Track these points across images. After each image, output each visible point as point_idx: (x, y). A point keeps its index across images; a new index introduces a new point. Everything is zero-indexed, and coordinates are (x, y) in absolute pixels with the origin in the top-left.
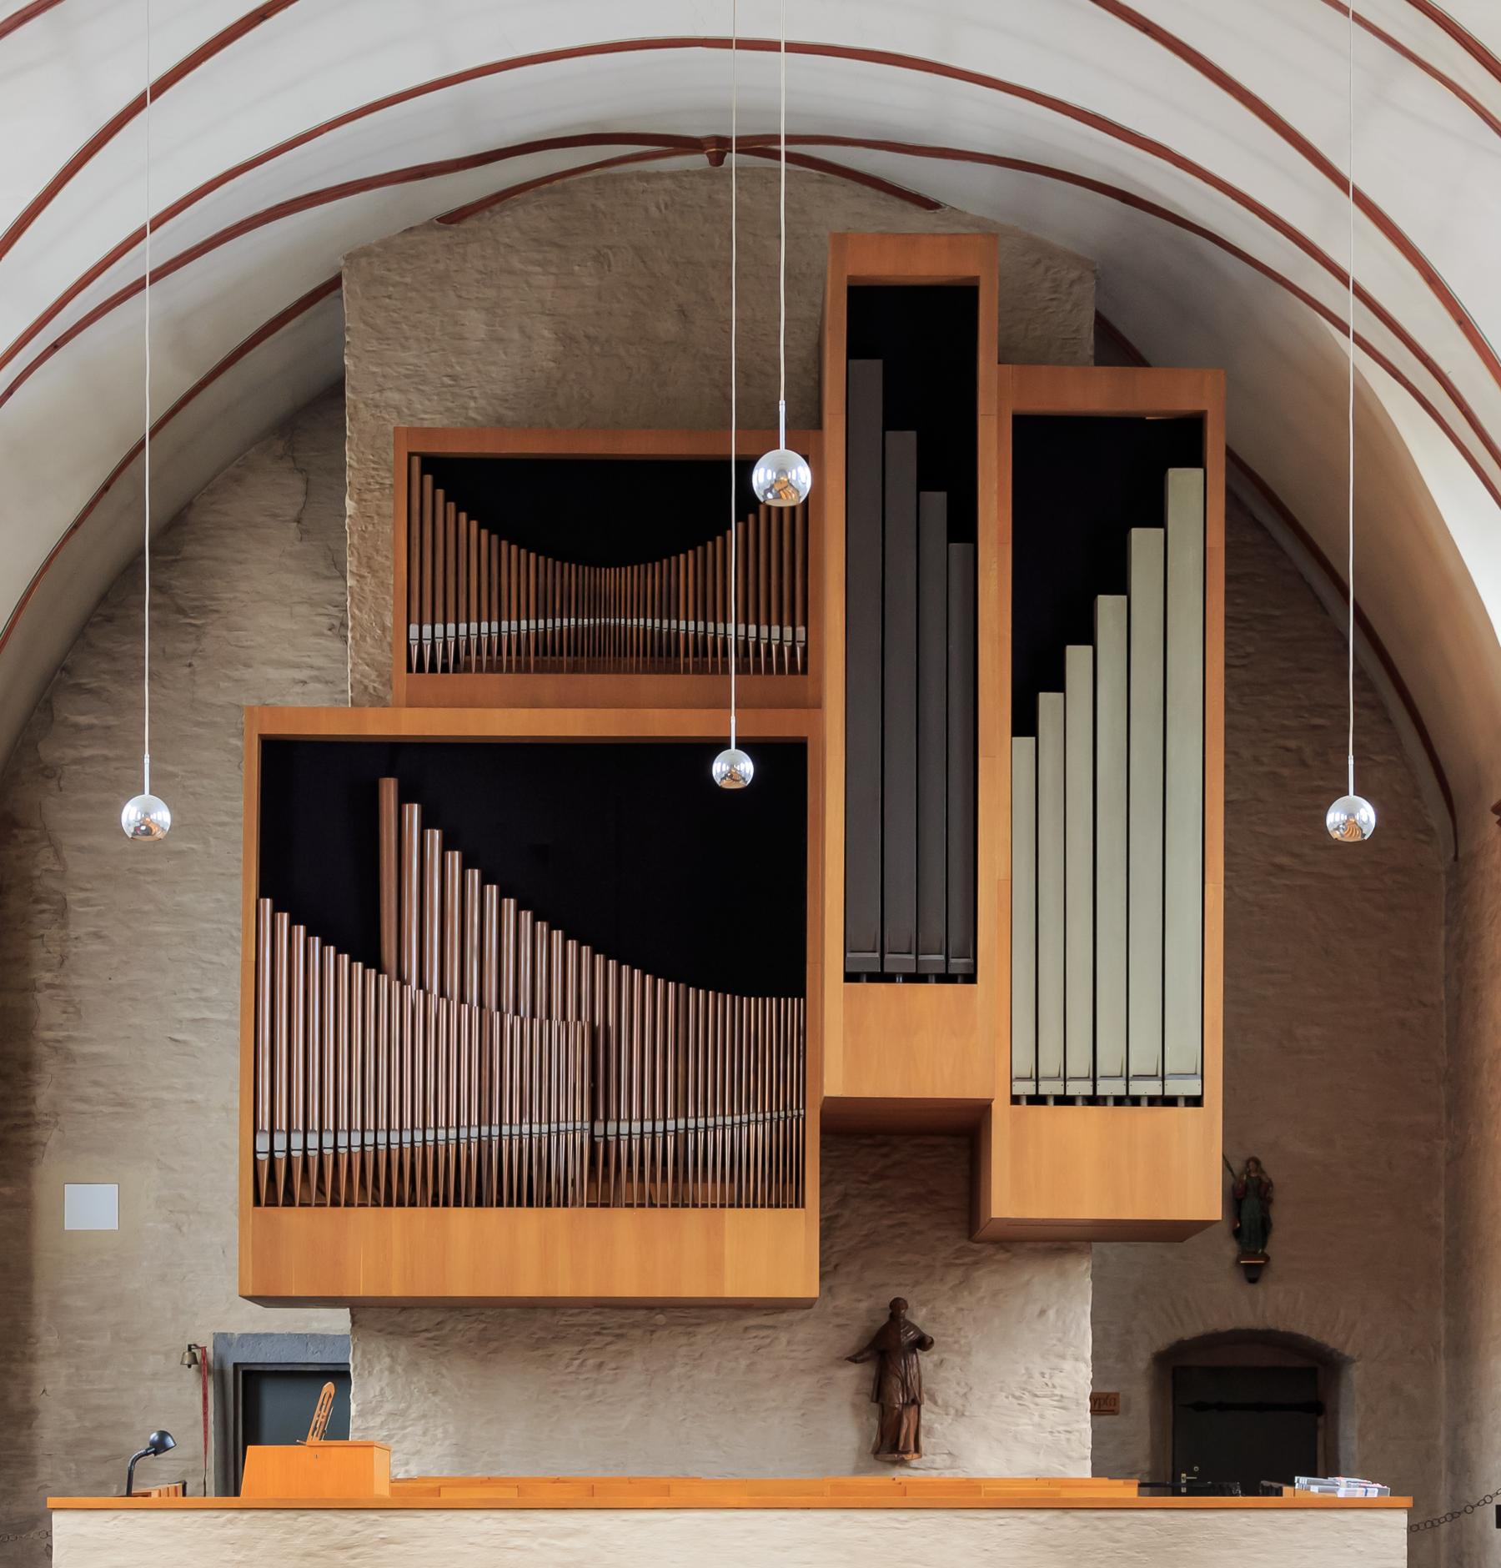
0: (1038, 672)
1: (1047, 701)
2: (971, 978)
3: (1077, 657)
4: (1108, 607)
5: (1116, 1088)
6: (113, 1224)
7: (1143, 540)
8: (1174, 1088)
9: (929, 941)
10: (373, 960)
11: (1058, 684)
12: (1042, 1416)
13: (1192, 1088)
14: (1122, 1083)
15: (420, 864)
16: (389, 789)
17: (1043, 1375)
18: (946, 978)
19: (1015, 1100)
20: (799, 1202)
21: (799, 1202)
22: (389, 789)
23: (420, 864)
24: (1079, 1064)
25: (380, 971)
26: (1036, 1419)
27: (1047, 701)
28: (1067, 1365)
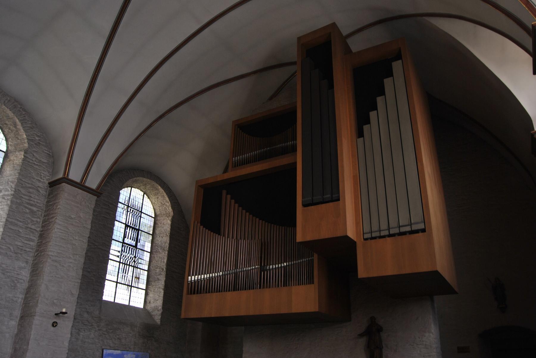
0: (362, 120)
1: (366, 128)
2: (339, 200)
3: (373, 115)
4: (380, 100)
5: (396, 231)
6: (141, 306)
7: (387, 82)
8: (415, 227)
9: (327, 191)
10: (219, 234)
11: (368, 122)
12: (420, 351)
13: (421, 226)
14: (398, 229)
15: (230, 208)
16: (224, 192)
17: (419, 338)
18: (332, 201)
19: (366, 239)
20: (313, 283)
21: (313, 283)
22: (224, 192)
23: (230, 208)
24: (384, 226)
25: (221, 236)
26: (419, 352)
27: (366, 128)
28: (427, 334)
